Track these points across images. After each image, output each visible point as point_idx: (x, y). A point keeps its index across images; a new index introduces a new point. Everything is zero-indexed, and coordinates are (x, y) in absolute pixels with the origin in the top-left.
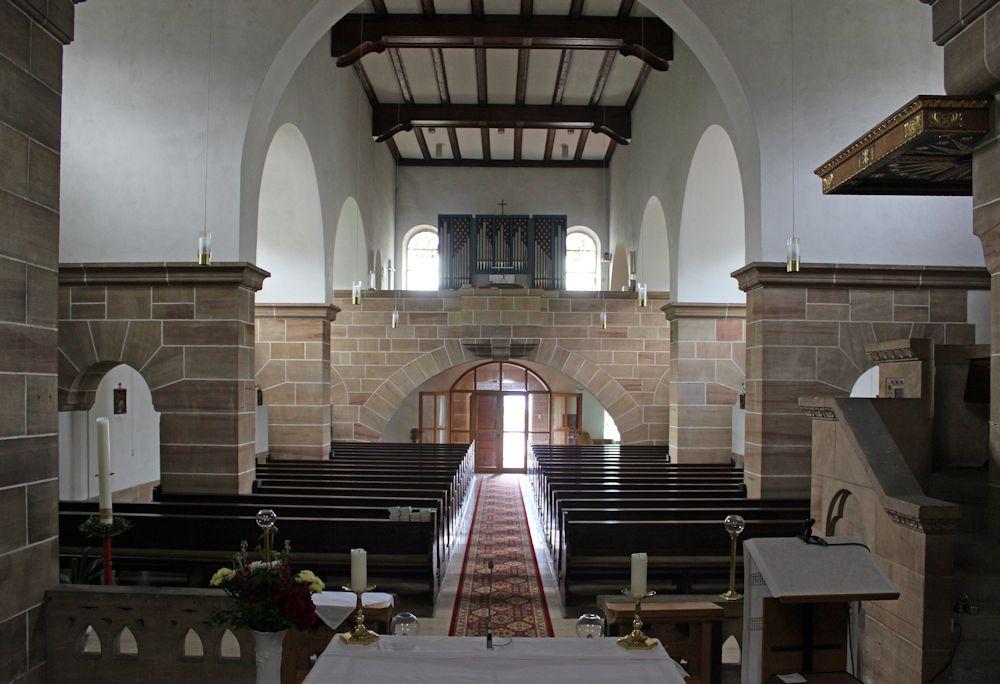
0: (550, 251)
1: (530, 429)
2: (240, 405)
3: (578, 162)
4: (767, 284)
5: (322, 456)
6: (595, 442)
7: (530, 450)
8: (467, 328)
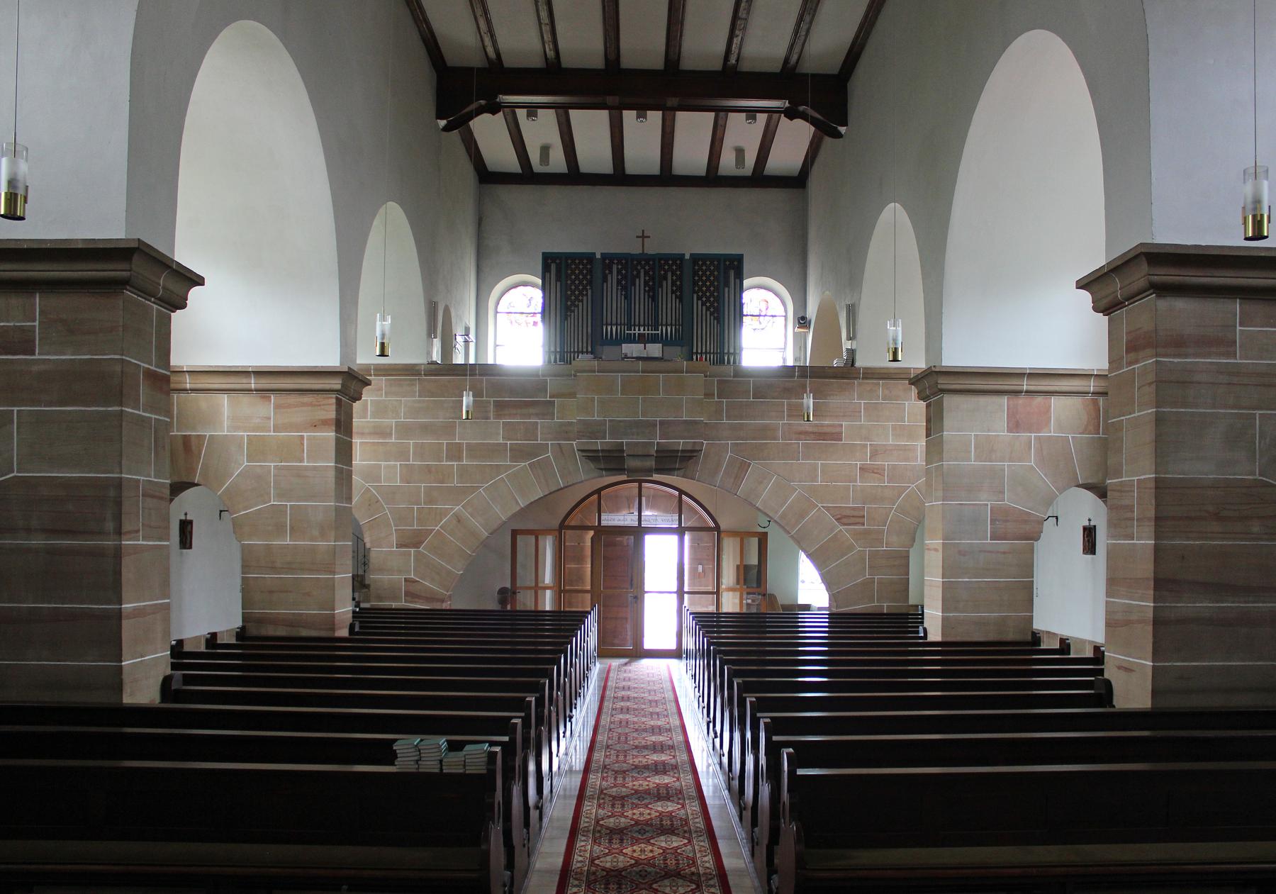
1: (686, 589)
2: (127, 526)
3: (760, 179)
4: (1163, 290)
5: (333, 630)
6: (784, 607)
7: (689, 621)
8: (585, 423)
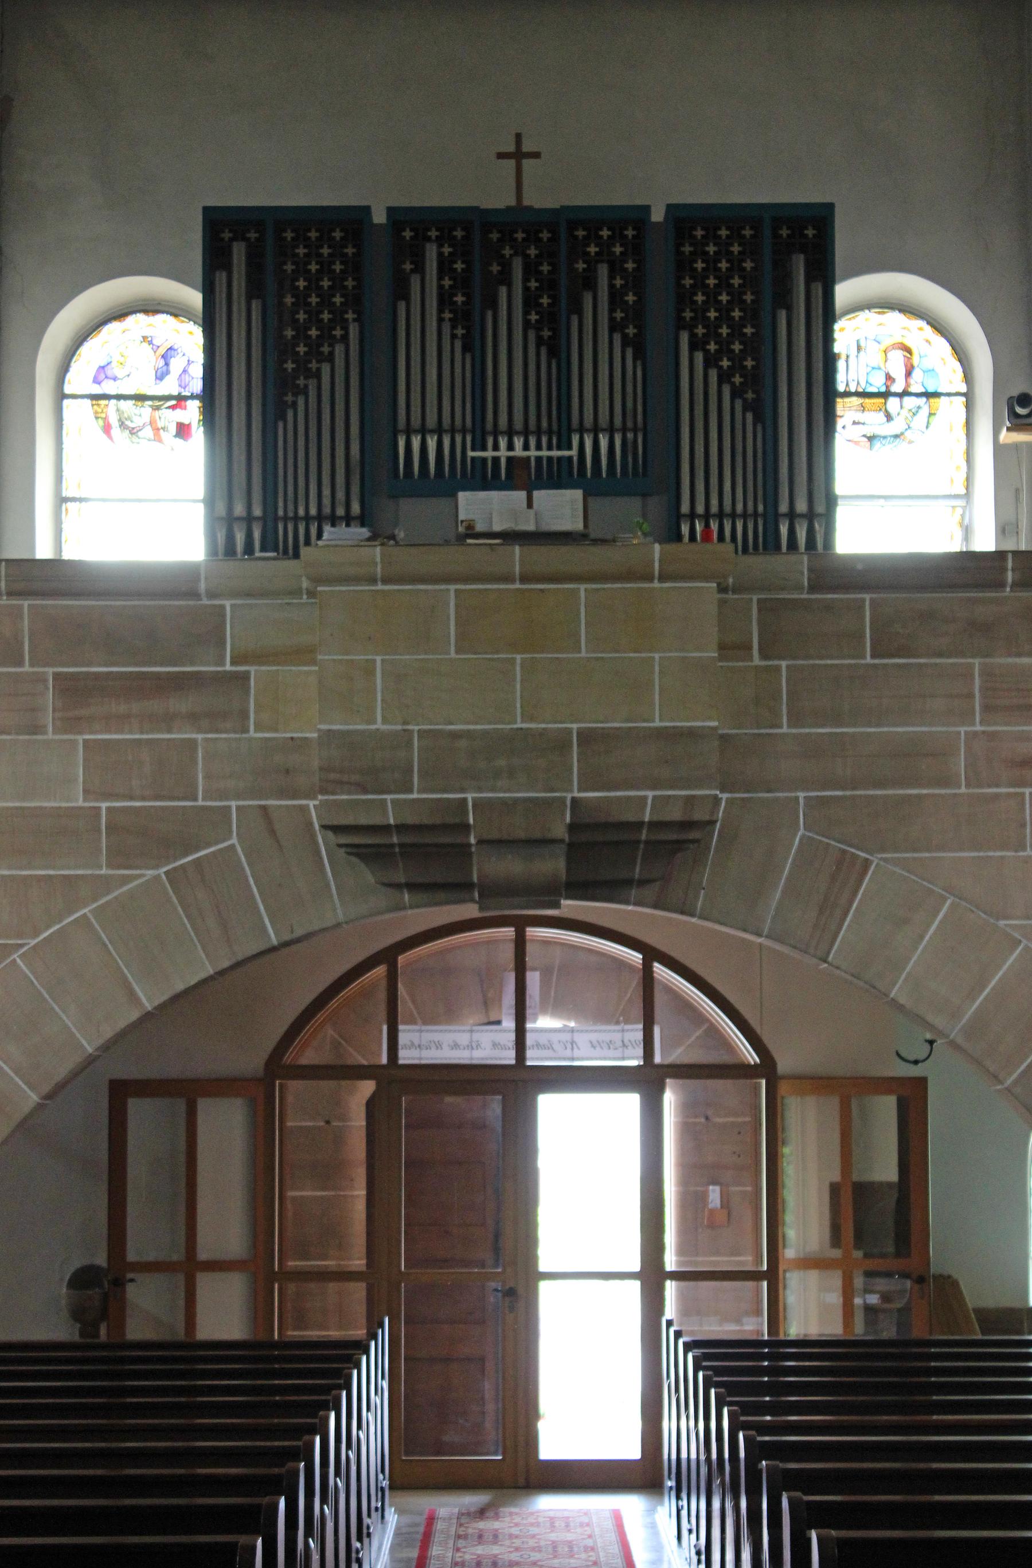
0: (754, 379)
1: (671, 1262)
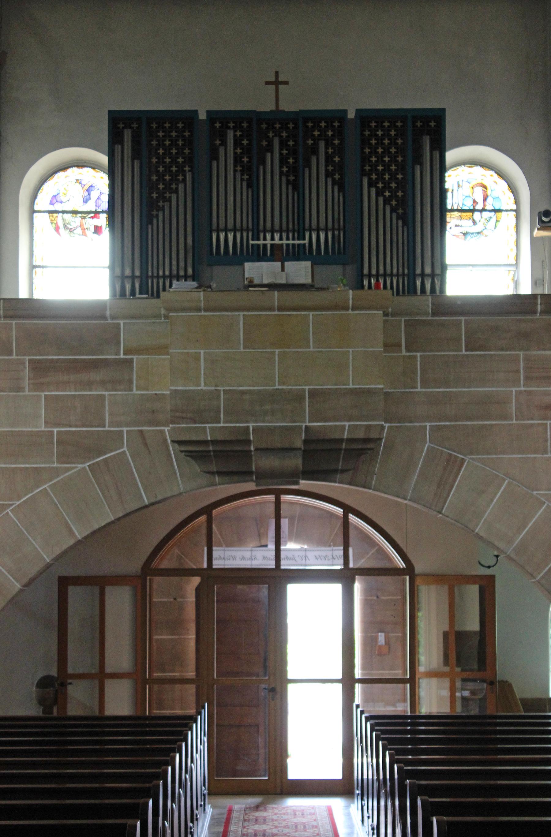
0: (402, 202)
1: (358, 673)
